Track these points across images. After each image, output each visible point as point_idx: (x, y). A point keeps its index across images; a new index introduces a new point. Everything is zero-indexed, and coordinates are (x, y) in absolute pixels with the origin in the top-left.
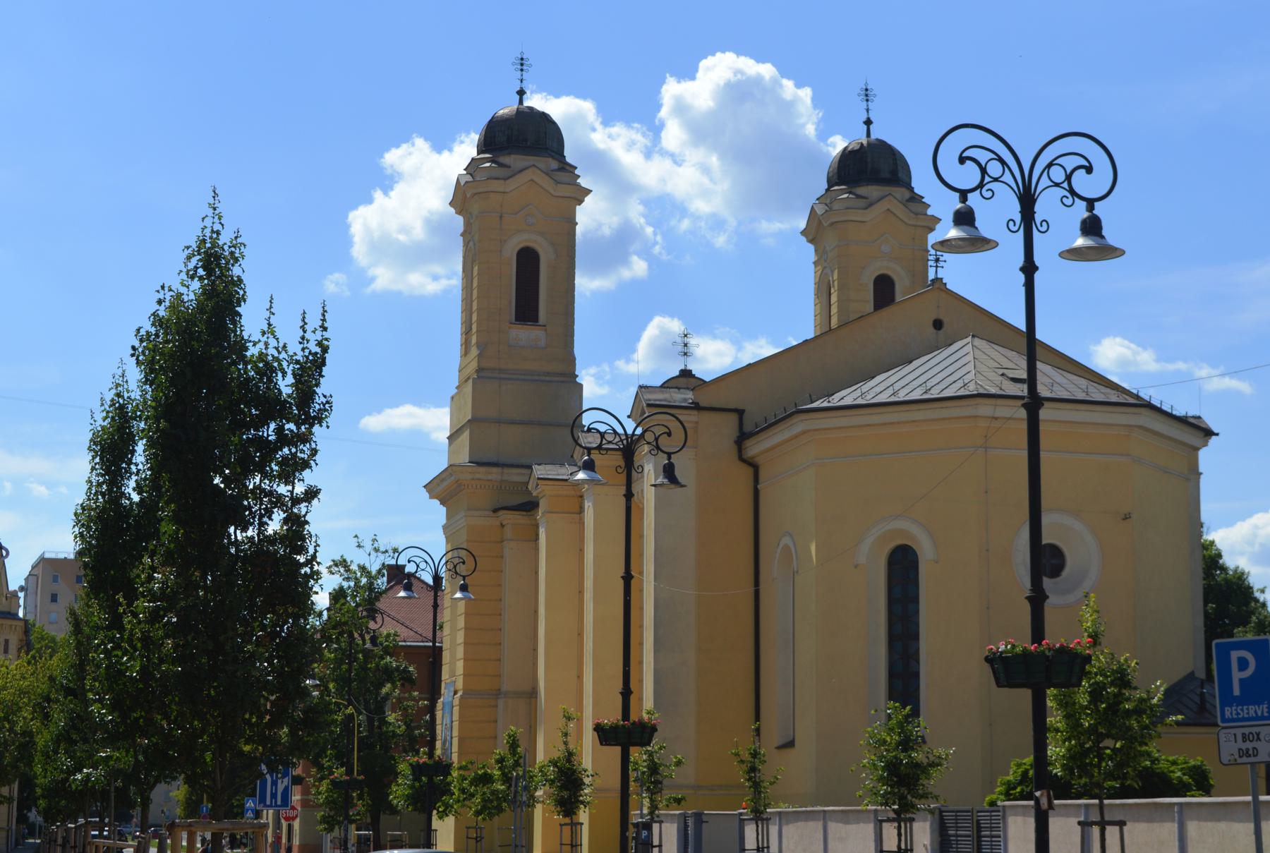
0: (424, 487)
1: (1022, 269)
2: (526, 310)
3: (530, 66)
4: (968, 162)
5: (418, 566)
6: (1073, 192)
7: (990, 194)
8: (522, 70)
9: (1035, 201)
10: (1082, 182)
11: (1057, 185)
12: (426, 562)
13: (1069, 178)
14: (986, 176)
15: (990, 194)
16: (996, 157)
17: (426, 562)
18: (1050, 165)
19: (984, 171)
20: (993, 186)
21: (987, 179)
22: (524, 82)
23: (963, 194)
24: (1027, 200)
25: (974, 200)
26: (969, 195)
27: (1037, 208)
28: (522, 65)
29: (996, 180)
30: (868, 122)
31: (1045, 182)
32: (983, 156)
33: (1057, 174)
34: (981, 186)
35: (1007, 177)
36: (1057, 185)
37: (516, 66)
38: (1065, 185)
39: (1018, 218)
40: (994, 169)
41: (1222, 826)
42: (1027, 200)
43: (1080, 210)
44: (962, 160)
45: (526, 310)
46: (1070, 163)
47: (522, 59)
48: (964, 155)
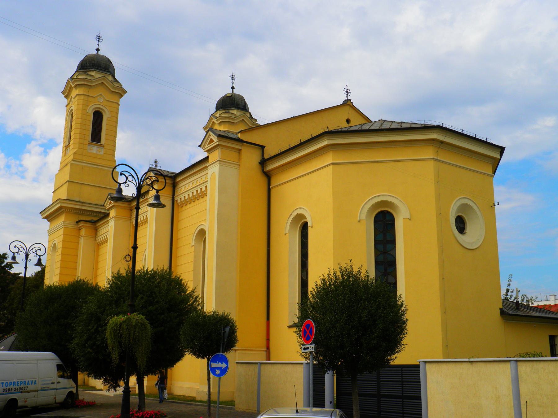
0: (40, 213)
1: (27, 268)
2: (96, 137)
3: (102, 40)
4: (16, 248)
5: (19, 250)
6: (36, 254)
7: (128, 185)
8: (99, 41)
9: (28, 256)
10: (38, 252)
11: (34, 253)
12: (133, 177)
13: (36, 251)
14: (127, 180)
15: (128, 185)
16: (131, 175)
17: (133, 177)
18: (33, 249)
19: (127, 178)
20: (20, 253)
21: (127, 181)
22: (99, 46)
23: (14, 253)
24: (27, 256)
25: (16, 255)
26: (15, 254)
27: (29, 257)
28: (99, 39)
29: (130, 182)
30: (98, 50)
31: (31, 252)
32: (19, 247)
33: (34, 251)
34: (125, 182)
35: (134, 181)
36: (34, 253)
37: (96, 39)
38: (35, 253)
39: (25, 259)
40: (21, 249)
41: (218, 387)
42: (27, 256)
43: (38, 257)
44: (15, 247)
45: (96, 137)
46: (37, 249)
47: (99, 37)
48: (122, 173)
